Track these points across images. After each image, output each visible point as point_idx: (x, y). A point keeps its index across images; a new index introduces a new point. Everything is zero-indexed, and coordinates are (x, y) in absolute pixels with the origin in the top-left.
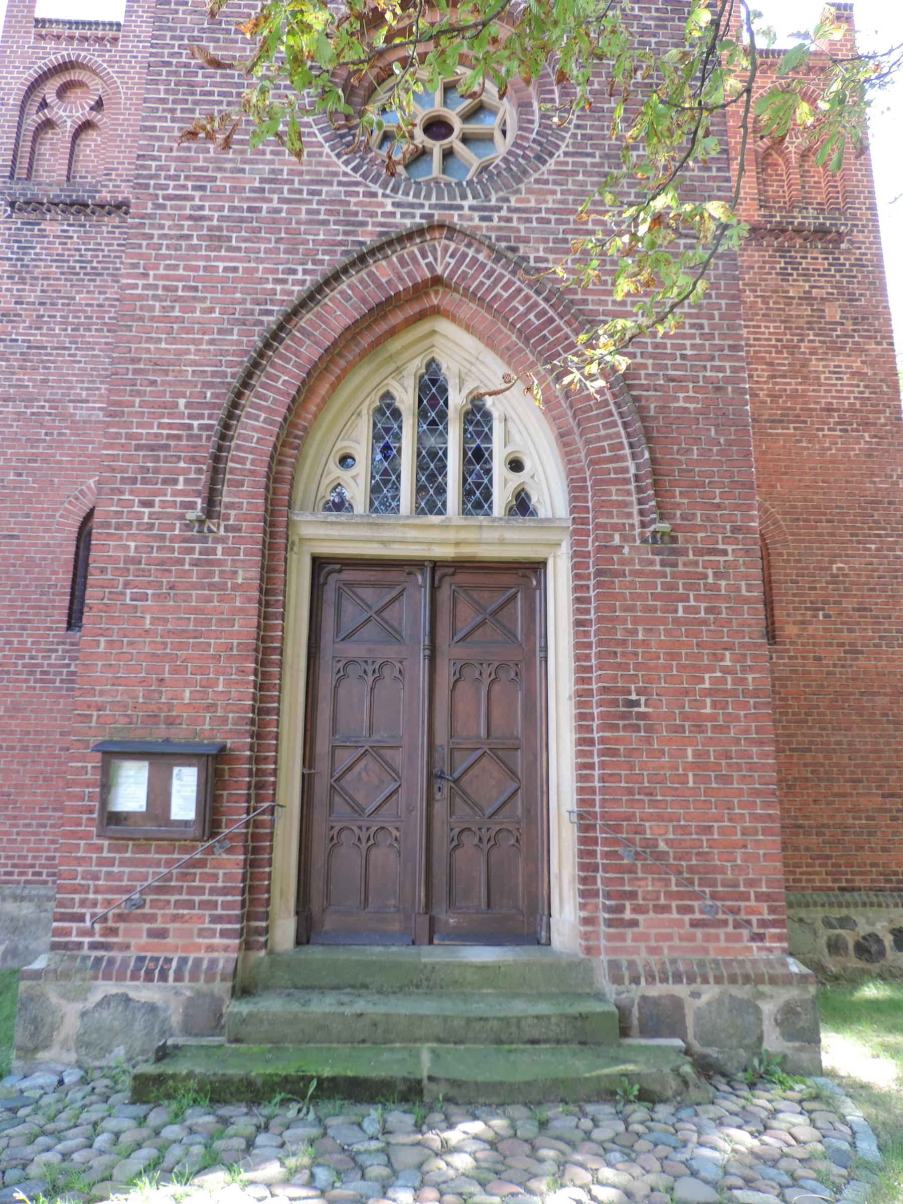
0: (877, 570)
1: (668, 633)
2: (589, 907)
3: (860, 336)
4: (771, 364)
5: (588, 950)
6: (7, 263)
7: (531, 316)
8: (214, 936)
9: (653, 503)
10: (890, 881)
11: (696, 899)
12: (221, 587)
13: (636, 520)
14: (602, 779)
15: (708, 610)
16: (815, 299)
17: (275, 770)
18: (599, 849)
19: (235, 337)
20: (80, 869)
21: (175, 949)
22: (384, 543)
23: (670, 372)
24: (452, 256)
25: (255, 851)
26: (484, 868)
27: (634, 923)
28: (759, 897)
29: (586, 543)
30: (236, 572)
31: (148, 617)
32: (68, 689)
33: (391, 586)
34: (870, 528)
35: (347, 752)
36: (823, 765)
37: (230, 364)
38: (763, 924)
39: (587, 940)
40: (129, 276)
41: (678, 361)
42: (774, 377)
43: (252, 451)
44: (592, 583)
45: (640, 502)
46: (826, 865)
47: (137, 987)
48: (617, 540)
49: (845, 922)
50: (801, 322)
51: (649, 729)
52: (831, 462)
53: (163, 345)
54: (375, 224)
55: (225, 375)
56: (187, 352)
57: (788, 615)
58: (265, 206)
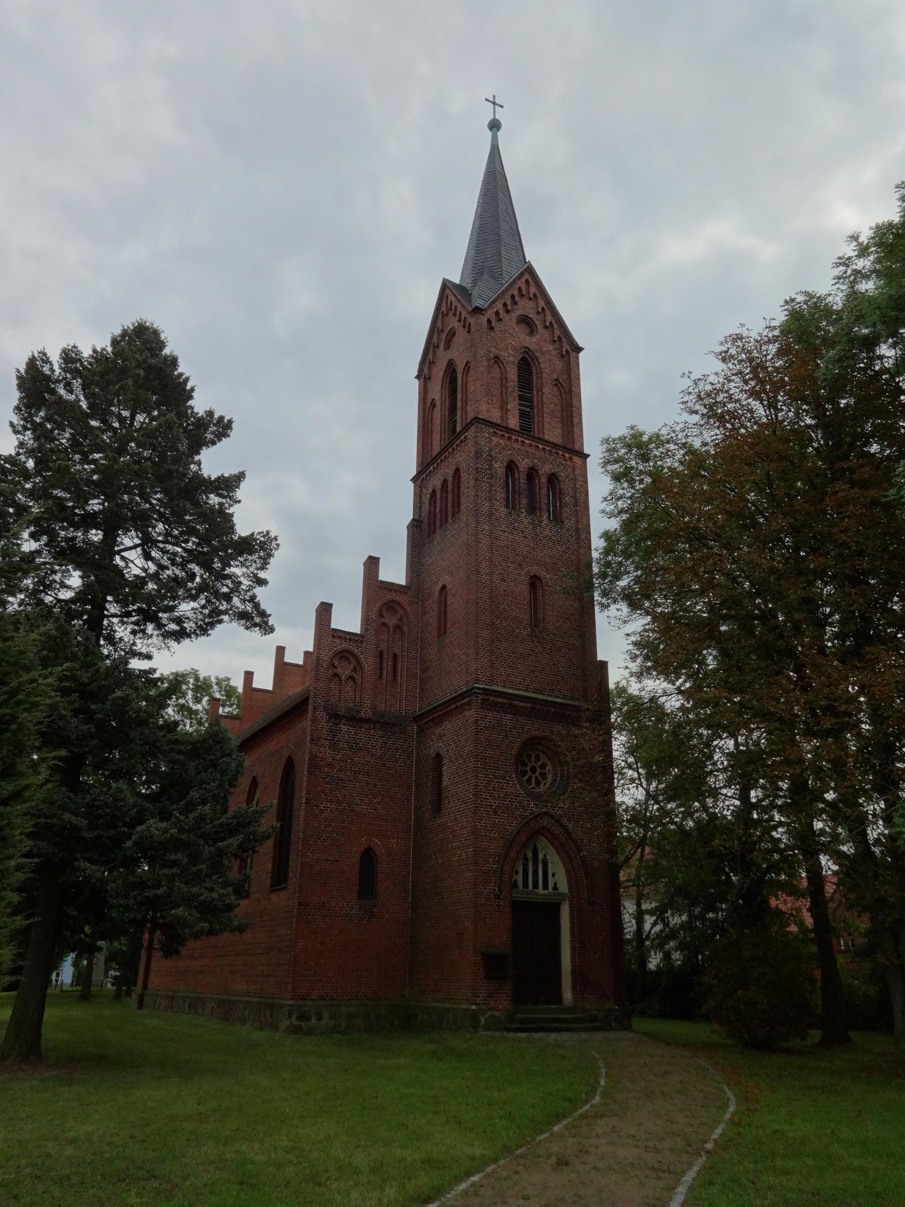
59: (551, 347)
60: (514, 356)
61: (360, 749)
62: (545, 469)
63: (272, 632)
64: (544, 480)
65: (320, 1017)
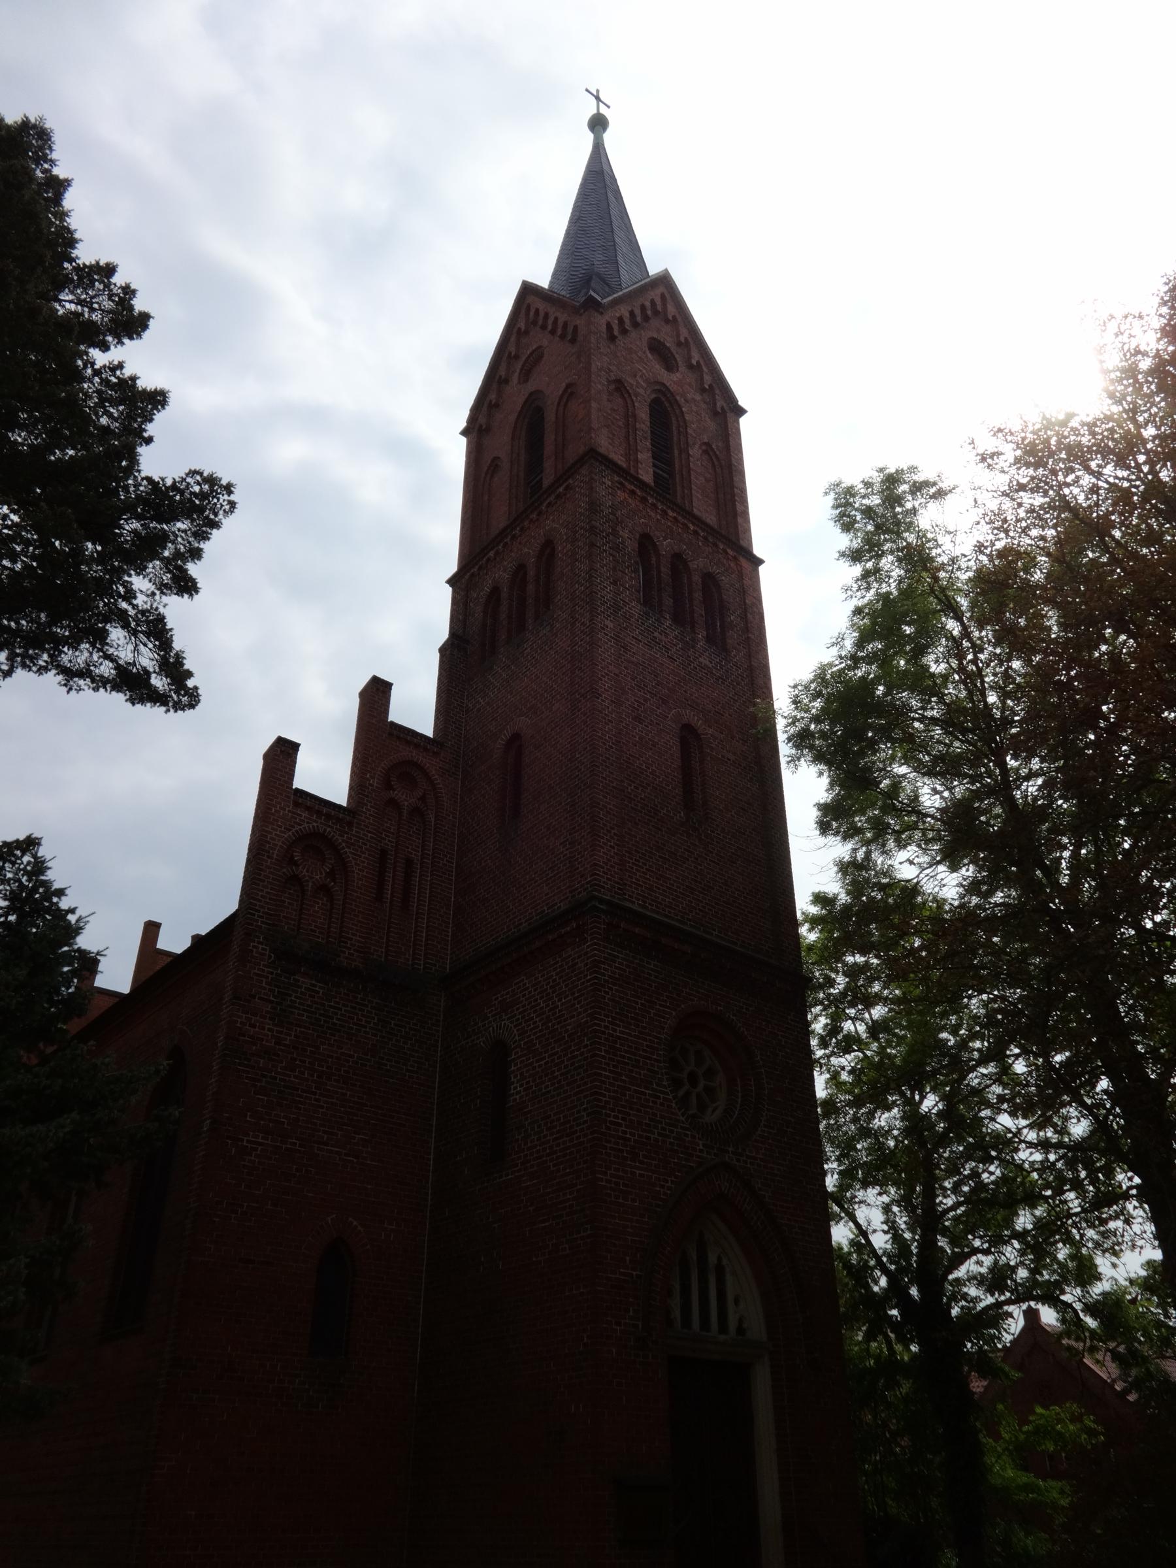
59: (698, 397)
60: (645, 389)
62: (698, 564)
63: (192, 706)
64: (696, 578)
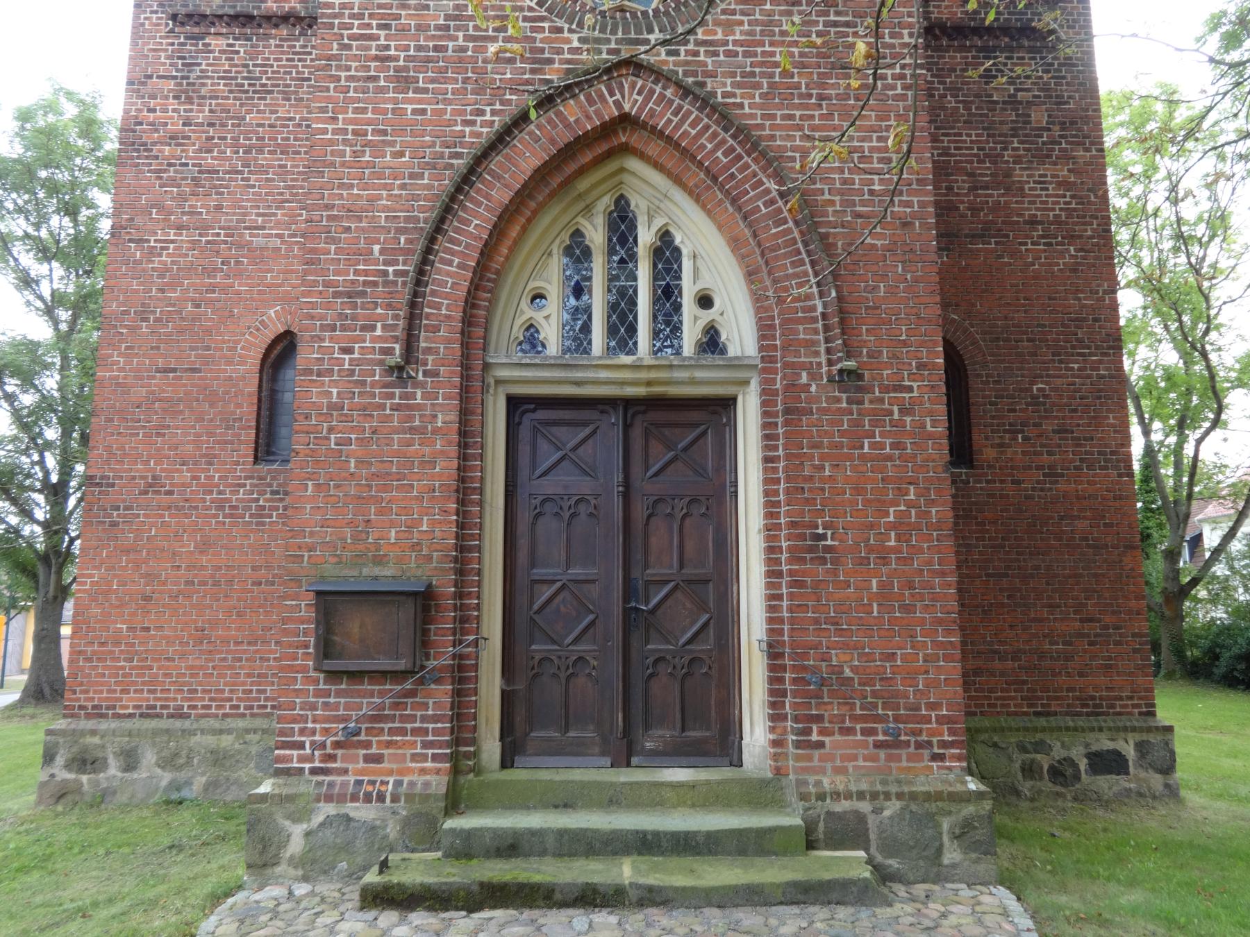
0: (1079, 390)
1: (853, 468)
2: (779, 731)
3: (1067, 143)
4: (971, 175)
5: (778, 772)
6: (173, 82)
7: (719, 154)
8: (426, 761)
9: (840, 342)
10: (1087, 706)
11: (880, 722)
12: (421, 431)
13: (823, 359)
14: (790, 610)
15: (893, 446)
16: (1020, 103)
17: (478, 604)
18: (787, 675)
19: (426, 181)
20: (298, 700)
21: (390, 773)
22: (578, 383)
23: (858, 208)
24: (639, 93)
25: (462, 680)
26: (677, 694)
27: (821, 745)
28: (940, 720)
29: (774, 381)
30: (436, 416)
31: (353, 461)
32: (258, 524)
33: (585, 424)
34: (1073, 347)
35: (545, 587)
36: (1020, 590)
37: (422, 209)
38: (943, 744)
39: (775, 761)
40: (319, 120)
41: (866, 197)
42: (976, 188)
43: (447, 296)
44: (780, 420)
45: (827, 341)
46: (1021, 690)
47: (357, 808)
48: (804, 378)
49: (1040, 747)
50: (1005, 128)
51: (835, 562)
52: (1034, 278)
53: (355, 191)
54: (562, 62)
55: (417, 220)
56: (380, 198)
57: (987, 438)
58: (451, 44)
61: (265, 91)
65: (130, 761)
